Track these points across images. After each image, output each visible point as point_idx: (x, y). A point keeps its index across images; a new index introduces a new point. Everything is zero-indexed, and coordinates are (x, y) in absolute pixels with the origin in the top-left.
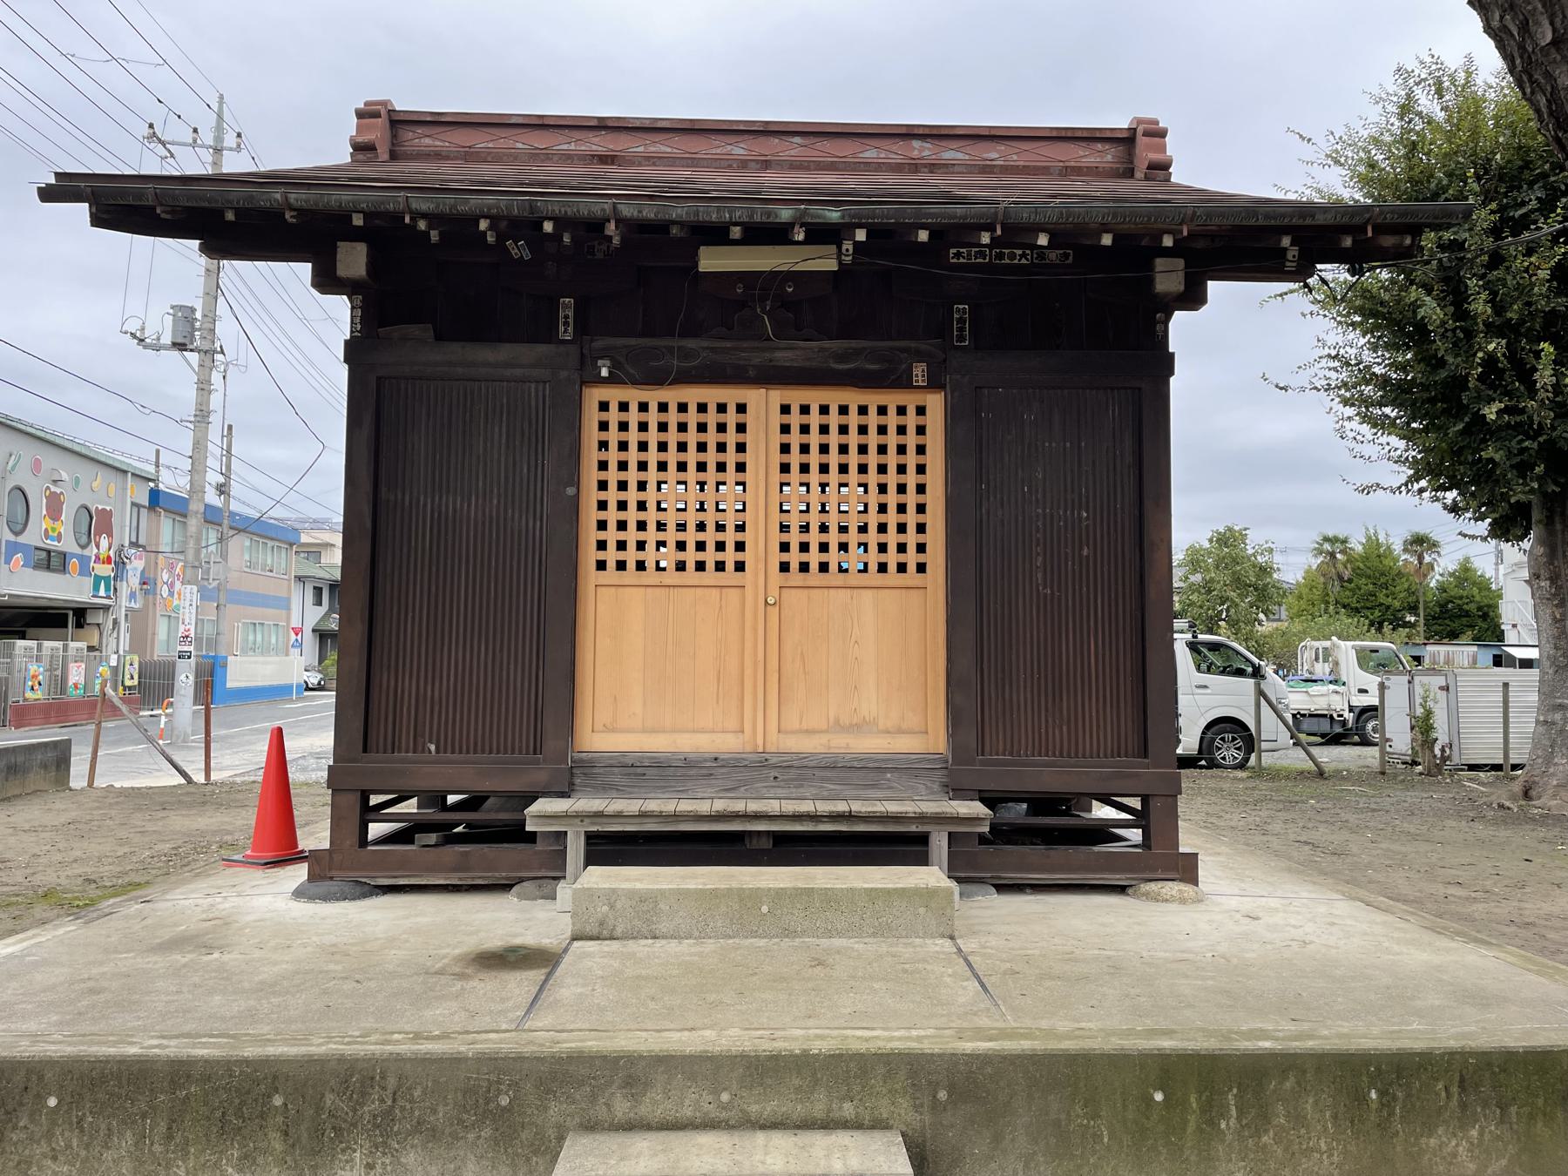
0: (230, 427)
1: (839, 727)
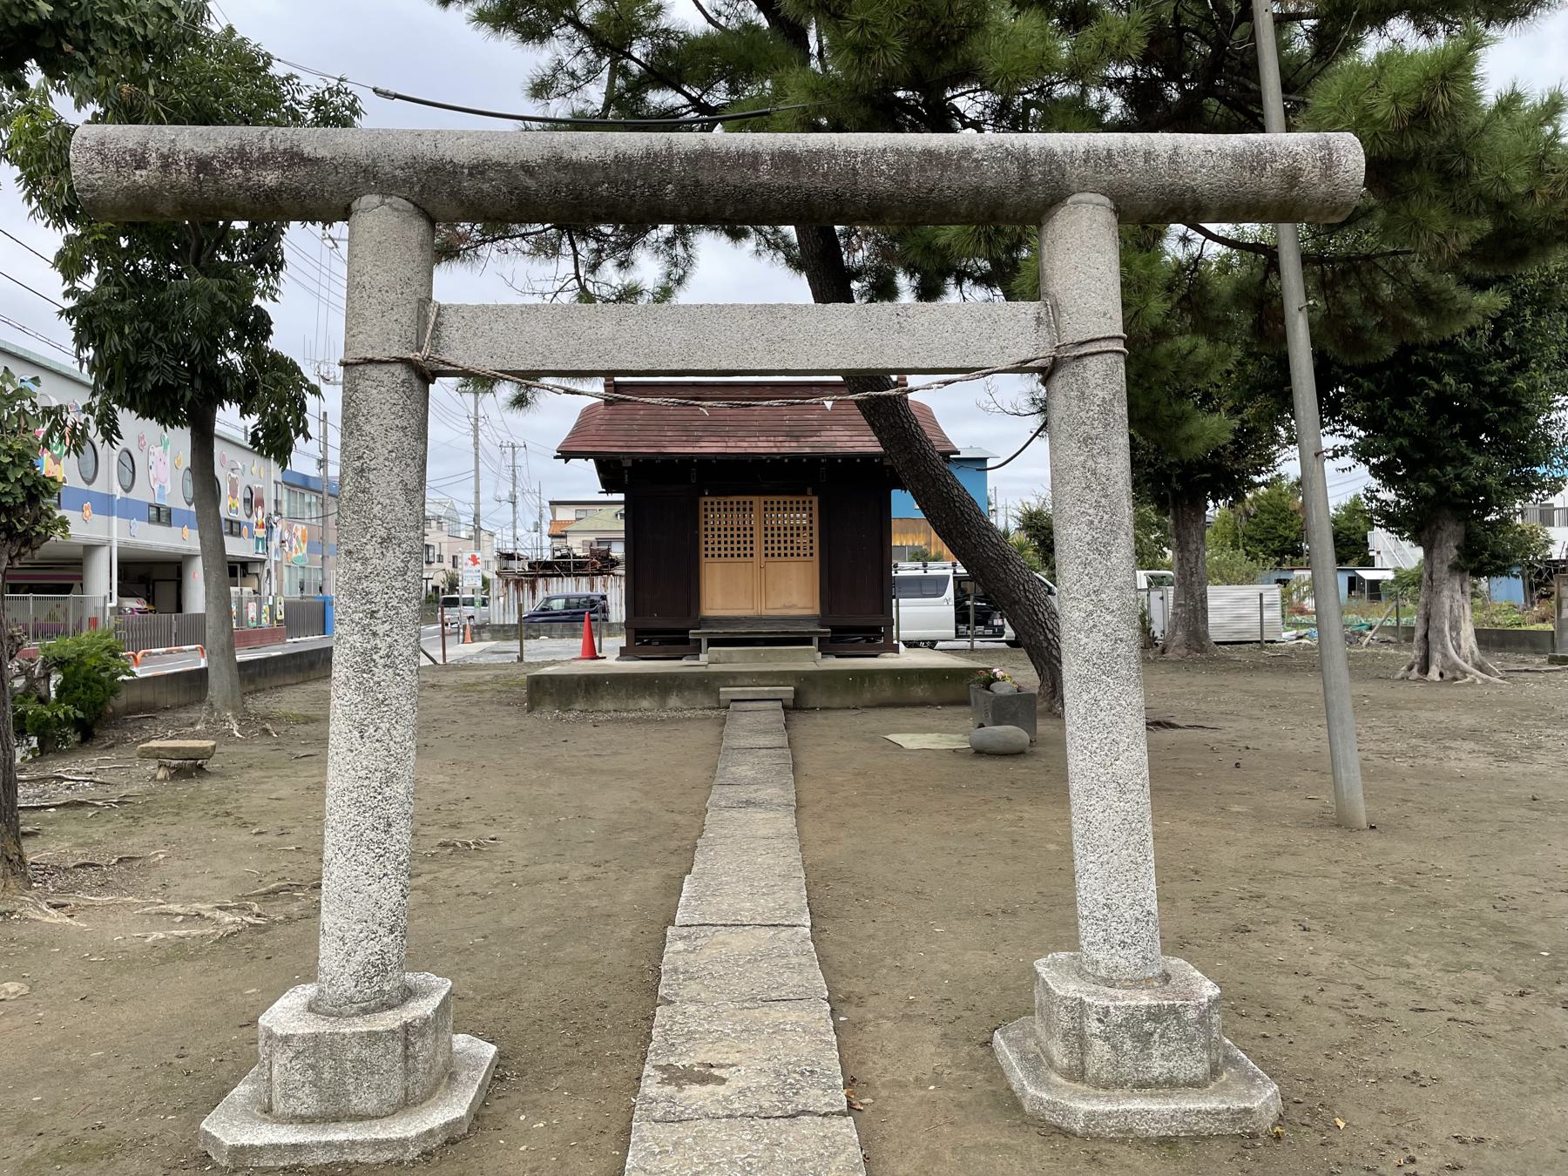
0: (325, 414)
1: (785, 607)
